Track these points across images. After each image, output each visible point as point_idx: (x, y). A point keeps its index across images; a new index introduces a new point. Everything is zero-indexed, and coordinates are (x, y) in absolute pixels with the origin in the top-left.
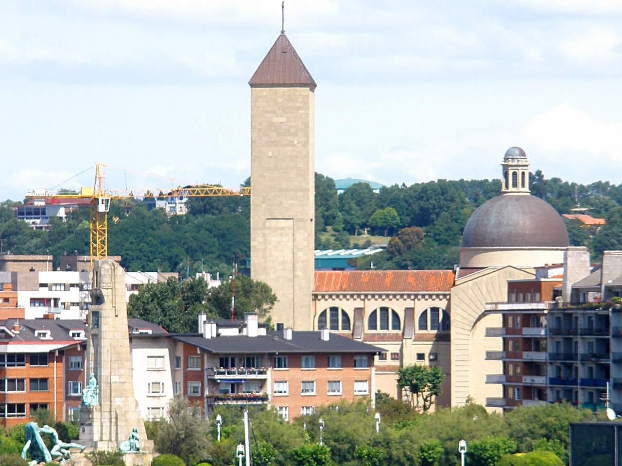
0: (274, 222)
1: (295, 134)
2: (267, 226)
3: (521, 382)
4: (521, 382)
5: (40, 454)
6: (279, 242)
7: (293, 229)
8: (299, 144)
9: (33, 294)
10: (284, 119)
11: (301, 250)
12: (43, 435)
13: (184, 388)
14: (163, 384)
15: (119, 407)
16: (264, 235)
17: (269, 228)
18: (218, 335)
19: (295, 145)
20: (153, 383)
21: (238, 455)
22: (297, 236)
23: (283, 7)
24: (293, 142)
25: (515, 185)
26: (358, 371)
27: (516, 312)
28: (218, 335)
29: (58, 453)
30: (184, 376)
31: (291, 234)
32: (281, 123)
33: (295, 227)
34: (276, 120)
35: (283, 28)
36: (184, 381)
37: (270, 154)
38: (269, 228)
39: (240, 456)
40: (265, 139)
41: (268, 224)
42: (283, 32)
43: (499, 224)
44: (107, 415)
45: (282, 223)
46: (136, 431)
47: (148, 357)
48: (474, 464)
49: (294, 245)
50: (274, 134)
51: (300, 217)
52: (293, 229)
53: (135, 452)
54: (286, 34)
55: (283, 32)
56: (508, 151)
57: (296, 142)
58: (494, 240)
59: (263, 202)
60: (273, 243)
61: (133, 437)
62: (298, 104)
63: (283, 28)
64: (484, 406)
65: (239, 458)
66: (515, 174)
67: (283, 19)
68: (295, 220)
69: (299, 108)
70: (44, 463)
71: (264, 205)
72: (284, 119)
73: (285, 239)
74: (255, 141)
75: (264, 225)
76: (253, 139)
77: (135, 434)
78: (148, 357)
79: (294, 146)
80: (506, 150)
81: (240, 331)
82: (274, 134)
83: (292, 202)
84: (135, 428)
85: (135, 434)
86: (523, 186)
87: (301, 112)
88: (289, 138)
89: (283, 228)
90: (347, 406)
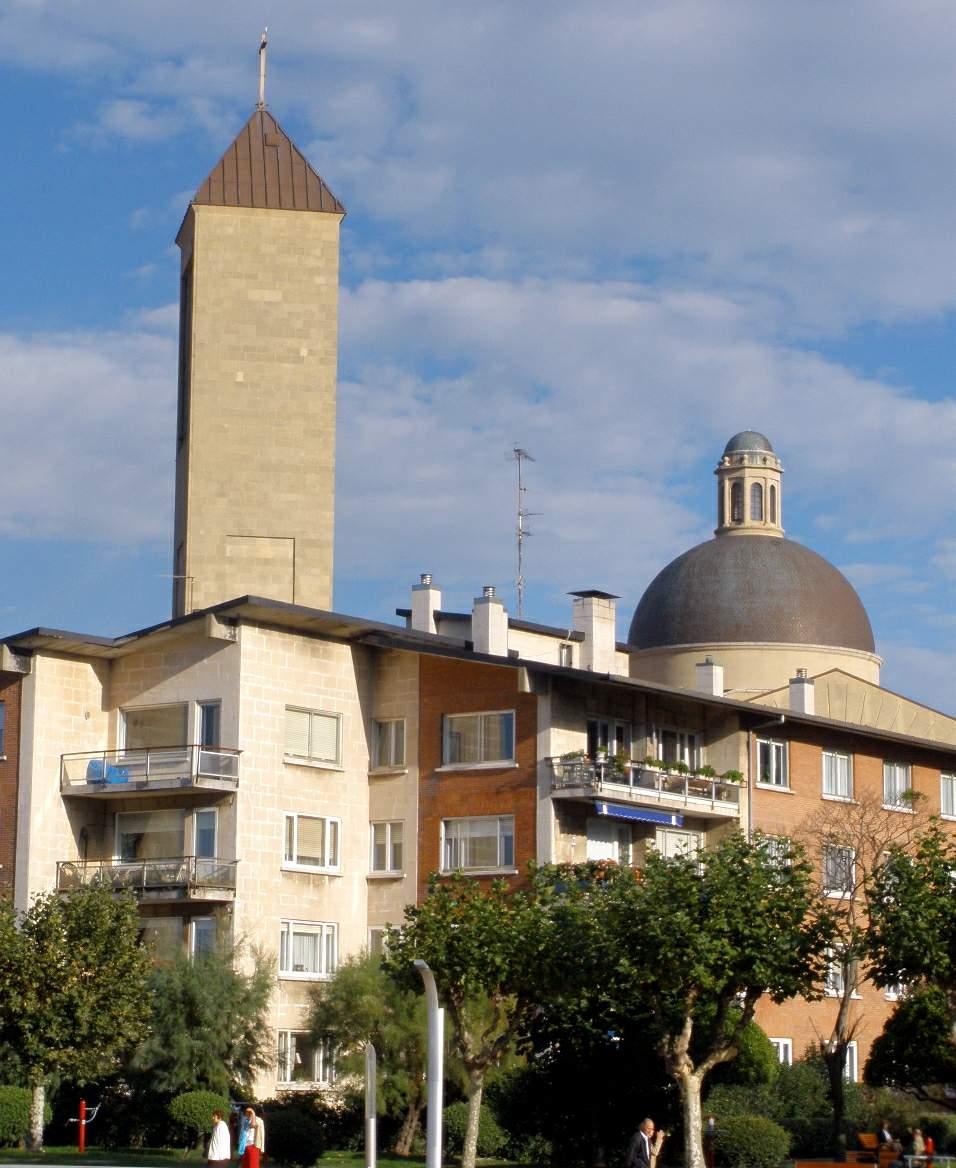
2: (228, 554)
8: (311, 358)
10: (274, 296)
14: (334, 824)
17: (231, 561)
20: (299, 817)
24: (297, 352)
25: (759, 515)
32: (269, 303)
34: (255, 295)
36: (423, 816)
37: (240, 377)
38: (231, 561)
47: (289, 708)
48: (669, 1135)
51: (313, 536)
57: (304, 352)
58: (738, 627)
59: (222, 495)
62: (311, 262)
70: (785, 1149)
72: (274, 296)
75: (221, 550)
78: (289, 708)
79: (299, 360)
80: (732, 436)
86: (773, 520)
88: (290, 342)
89: (267, 562)
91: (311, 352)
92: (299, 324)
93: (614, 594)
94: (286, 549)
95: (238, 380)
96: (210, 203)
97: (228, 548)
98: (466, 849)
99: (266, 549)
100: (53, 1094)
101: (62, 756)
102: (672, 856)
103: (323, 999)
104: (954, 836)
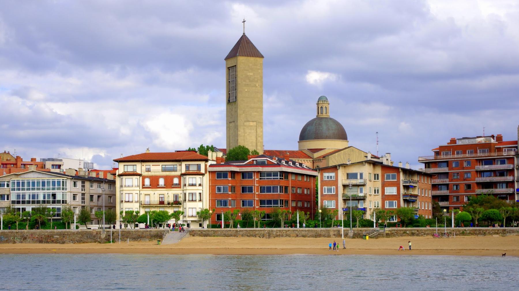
1: (257, 82)
3: (475, 192)
4: (475, 192)
6: (250, 133)
7: (256, 126)
9: (53, 163)
10: (251, 74)
11: (260, 137)
12: (282, 217)
13: (382, 191)
16: (244, 129)
19: (257, 86)
22: (258, 130)
24: (256, 85)
30: (382, 185)
31: (255, 129)
33: (257, 126)
34: (248, 74)
40: (244, 83)
49: (256, 134)
50: (248, 81)
51: (259, 121)
52: (256, 126)
56: (321, 97)
57: (257, 85)
58: (327, 136)
60: (247, 133)
64: (139, 224)
66: (321, 107)
67: (244, 28)
68: (257, 122)
69: (259, 69)
71: (244, 114)
72: (251, 74)
73: (253, 131)
75: (244, 124)
83: (255, 113)
87: (259, 71)
89: (252, 126)
90: (278, 212)
91: (258, 85)
92: (256, 80)
93: (324, 148)
94: (255, 123)
95: (426, 196)
96: (240, 56)
97: (245, 123)
98: (334, 204)
99: (252, 124)
100: (382, 223)
101: (132, 194)
102: (141, 234)
103: (356, 232)
104: (2, 197)
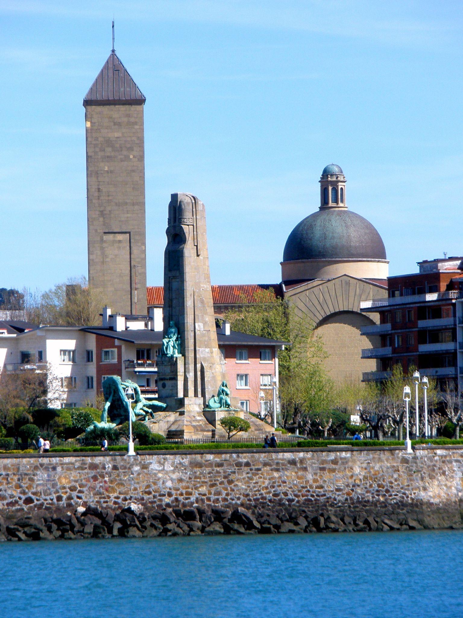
0: (111, 236)
5: (123, 413)
6: (116, 255)
15: (204, 359)
18: (127, 328)
21: (405, 398)
23: (113, 26)
26: (262, 365)
27: (408, 306)
28: (127, 328)
29: (142, 412)
35: (113, 47)
37: (106, 169)
39: (407, 399)
40: (101, 154)
41: (105, 237)
42: (113, 51)
43: (325, 237)
44: (191, 367)
45: (120, 237)
46: (226, 386)
53: (226, 409)
54: (116, 53)
55: (113, 51)
56: (328, 166)
57: (131, 157)
60: (110, 256)
61: (223, 391)
63: (113, 47)
65: (406, 401)
74: (91, 156)
76: (89, 154)
77: (225, 388)
81: (146, 325)
82: (110, 149)
84: (225, 382)
85: (225, 388)
89: (120, 241)
